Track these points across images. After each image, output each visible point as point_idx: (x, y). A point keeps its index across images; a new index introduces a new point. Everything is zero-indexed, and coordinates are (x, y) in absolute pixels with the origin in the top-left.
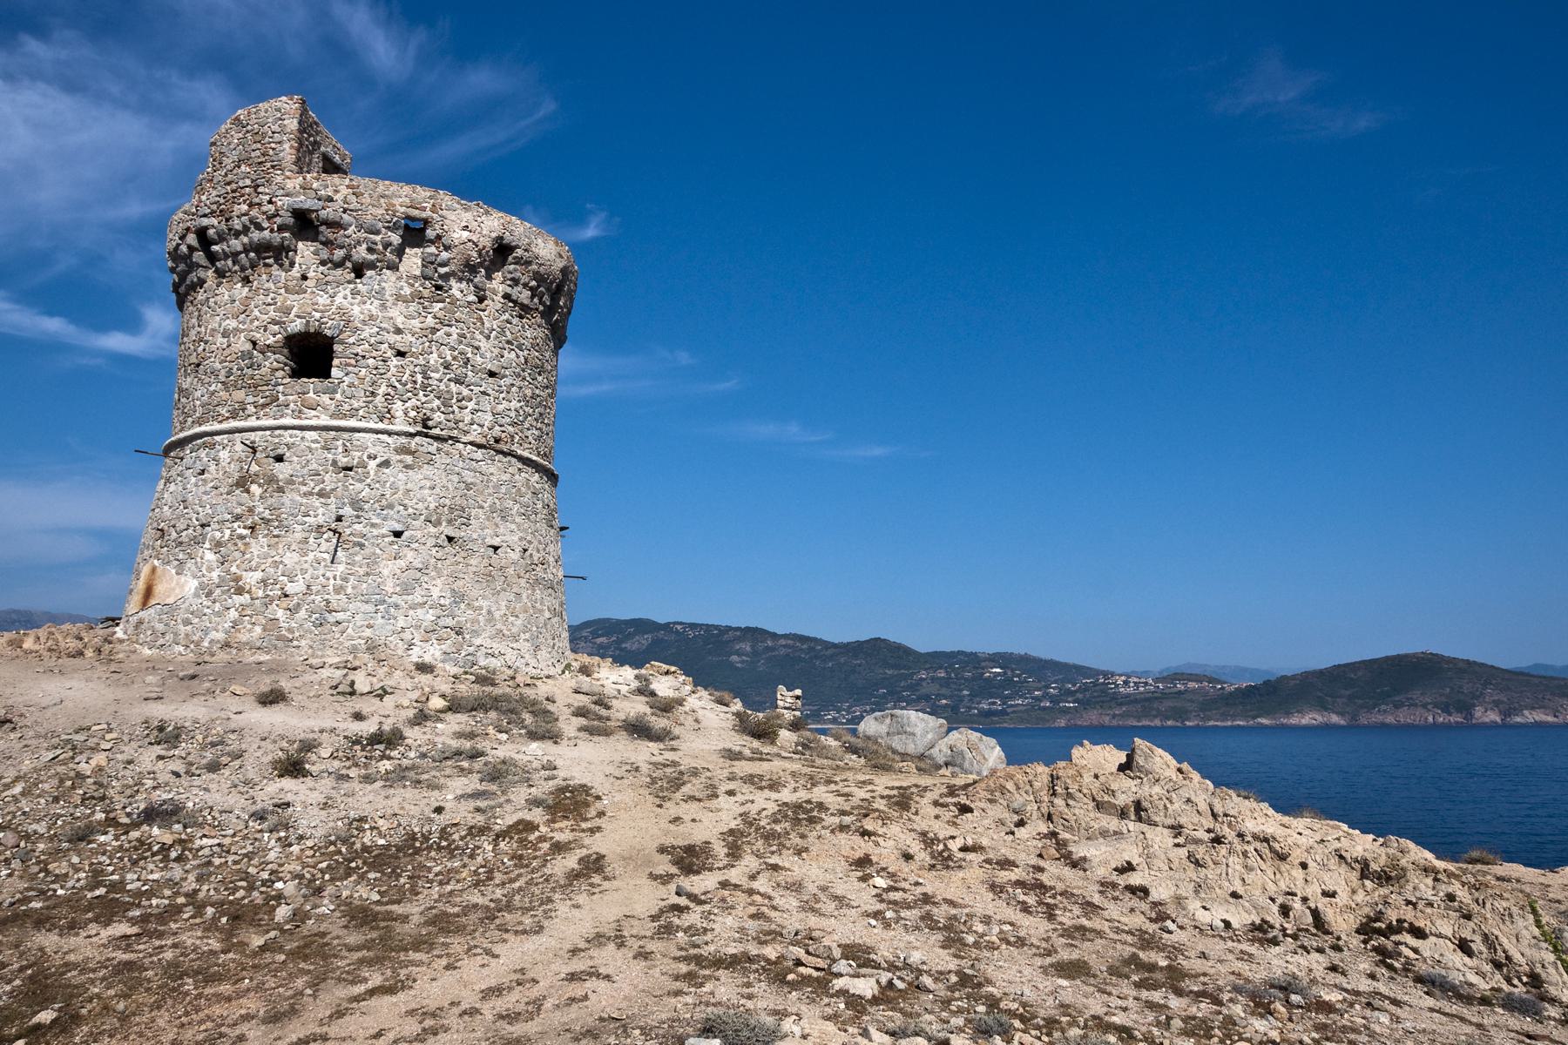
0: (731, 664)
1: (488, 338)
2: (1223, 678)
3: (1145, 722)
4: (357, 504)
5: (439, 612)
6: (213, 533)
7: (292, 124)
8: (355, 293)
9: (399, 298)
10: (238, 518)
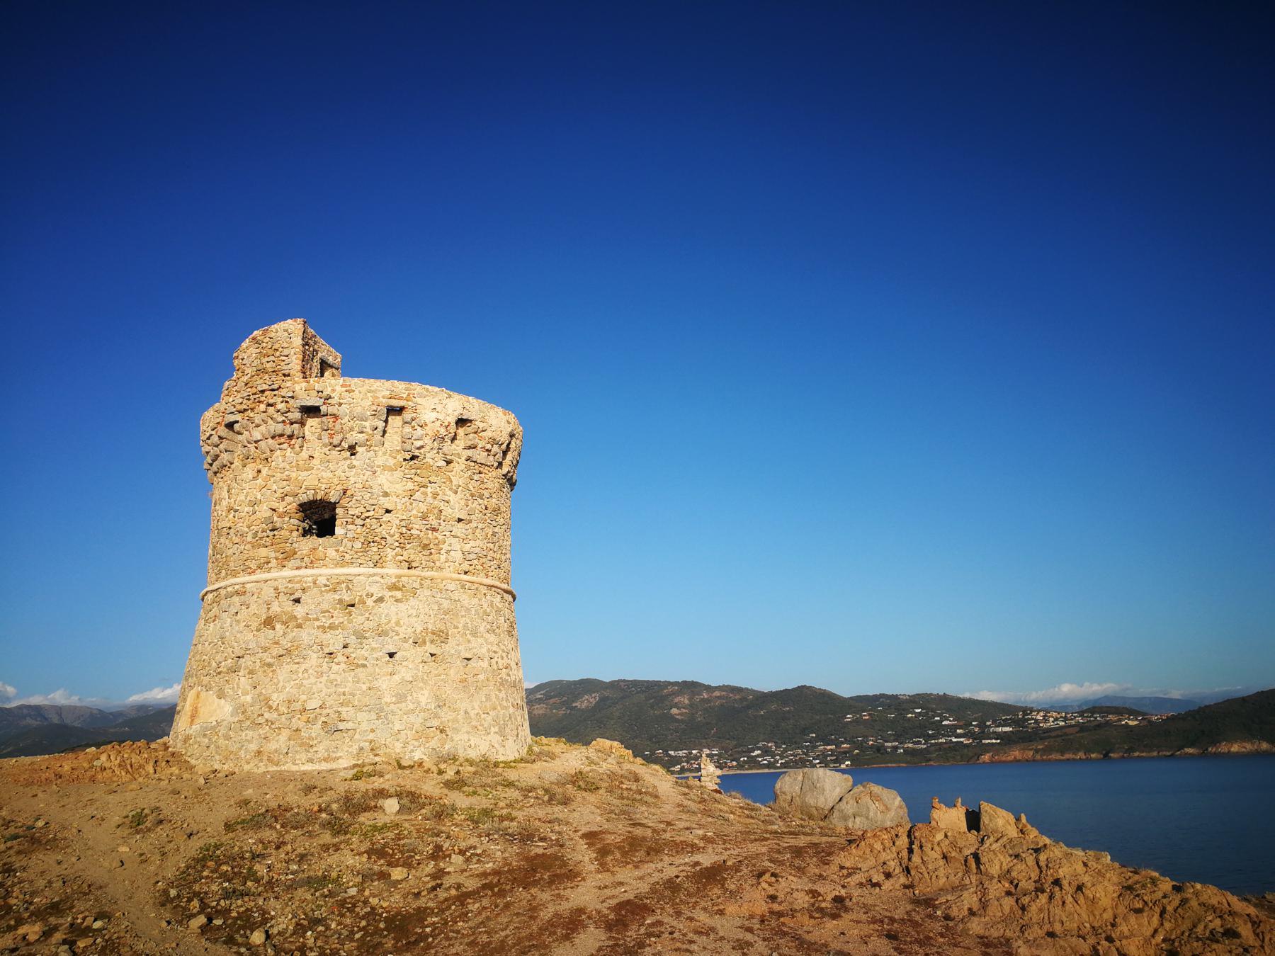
0: (672, 718)
1: (456, 493)
2: (1144, 709)
3: (1067, 756)
4: (361, 636)
5: (426, 715)
6: (246, 662)
7: (298, 341)
8: (351, 467)
9: (385, 468)
10: (265, 650)
